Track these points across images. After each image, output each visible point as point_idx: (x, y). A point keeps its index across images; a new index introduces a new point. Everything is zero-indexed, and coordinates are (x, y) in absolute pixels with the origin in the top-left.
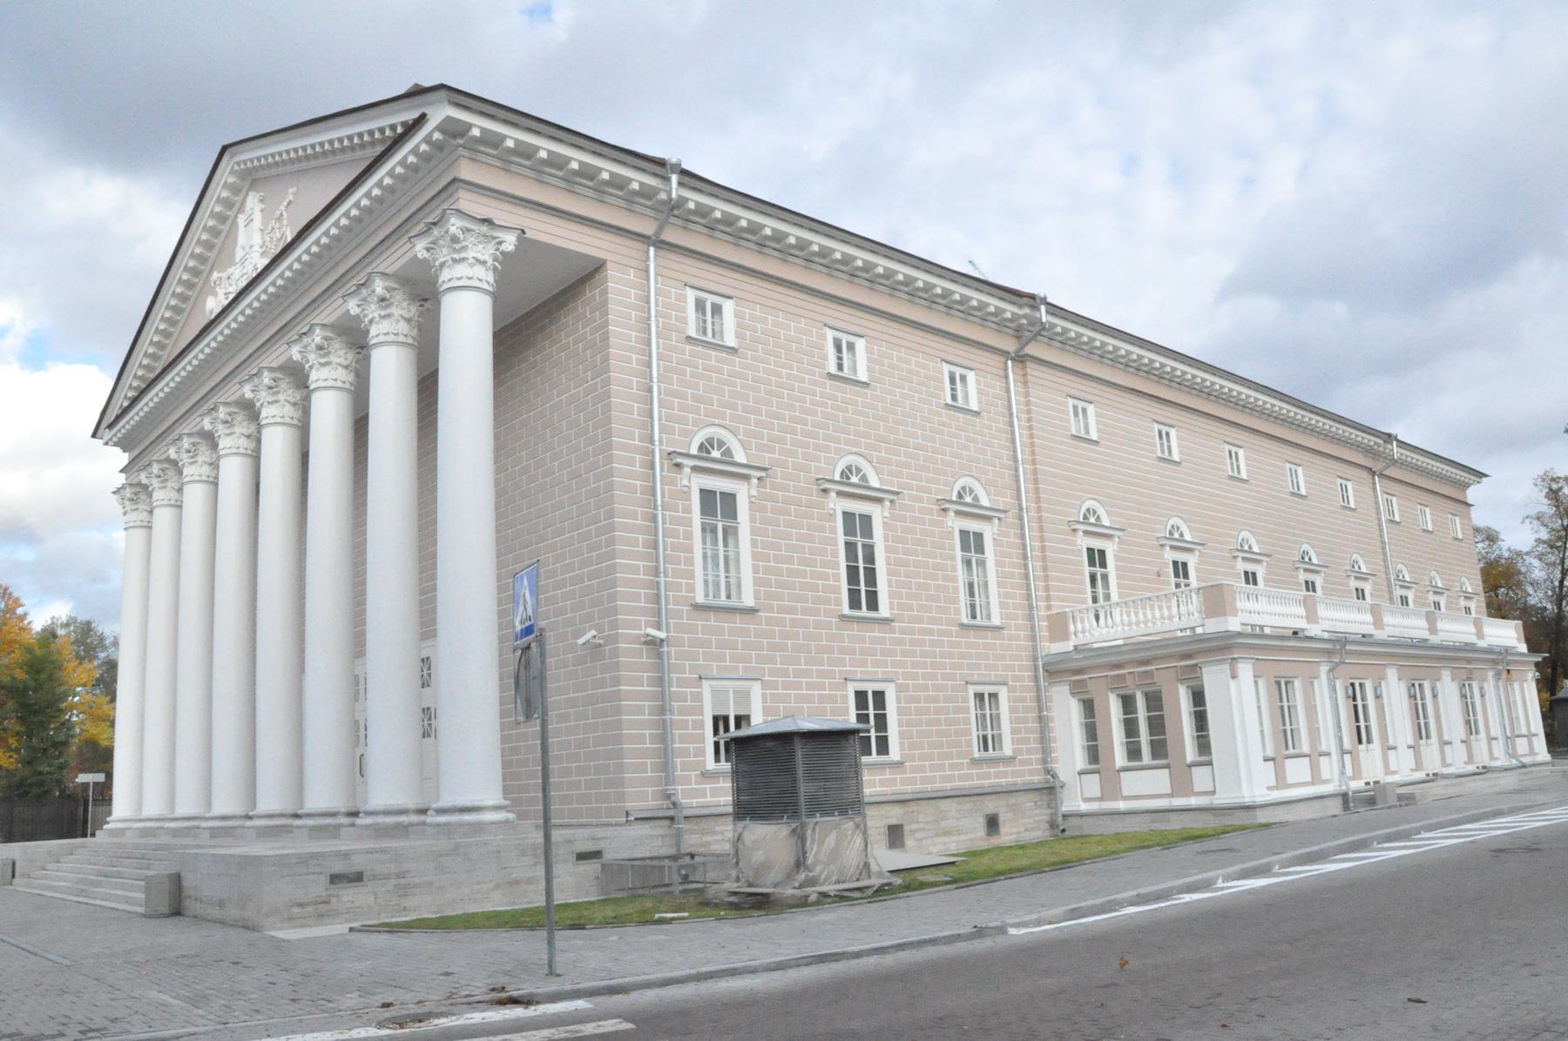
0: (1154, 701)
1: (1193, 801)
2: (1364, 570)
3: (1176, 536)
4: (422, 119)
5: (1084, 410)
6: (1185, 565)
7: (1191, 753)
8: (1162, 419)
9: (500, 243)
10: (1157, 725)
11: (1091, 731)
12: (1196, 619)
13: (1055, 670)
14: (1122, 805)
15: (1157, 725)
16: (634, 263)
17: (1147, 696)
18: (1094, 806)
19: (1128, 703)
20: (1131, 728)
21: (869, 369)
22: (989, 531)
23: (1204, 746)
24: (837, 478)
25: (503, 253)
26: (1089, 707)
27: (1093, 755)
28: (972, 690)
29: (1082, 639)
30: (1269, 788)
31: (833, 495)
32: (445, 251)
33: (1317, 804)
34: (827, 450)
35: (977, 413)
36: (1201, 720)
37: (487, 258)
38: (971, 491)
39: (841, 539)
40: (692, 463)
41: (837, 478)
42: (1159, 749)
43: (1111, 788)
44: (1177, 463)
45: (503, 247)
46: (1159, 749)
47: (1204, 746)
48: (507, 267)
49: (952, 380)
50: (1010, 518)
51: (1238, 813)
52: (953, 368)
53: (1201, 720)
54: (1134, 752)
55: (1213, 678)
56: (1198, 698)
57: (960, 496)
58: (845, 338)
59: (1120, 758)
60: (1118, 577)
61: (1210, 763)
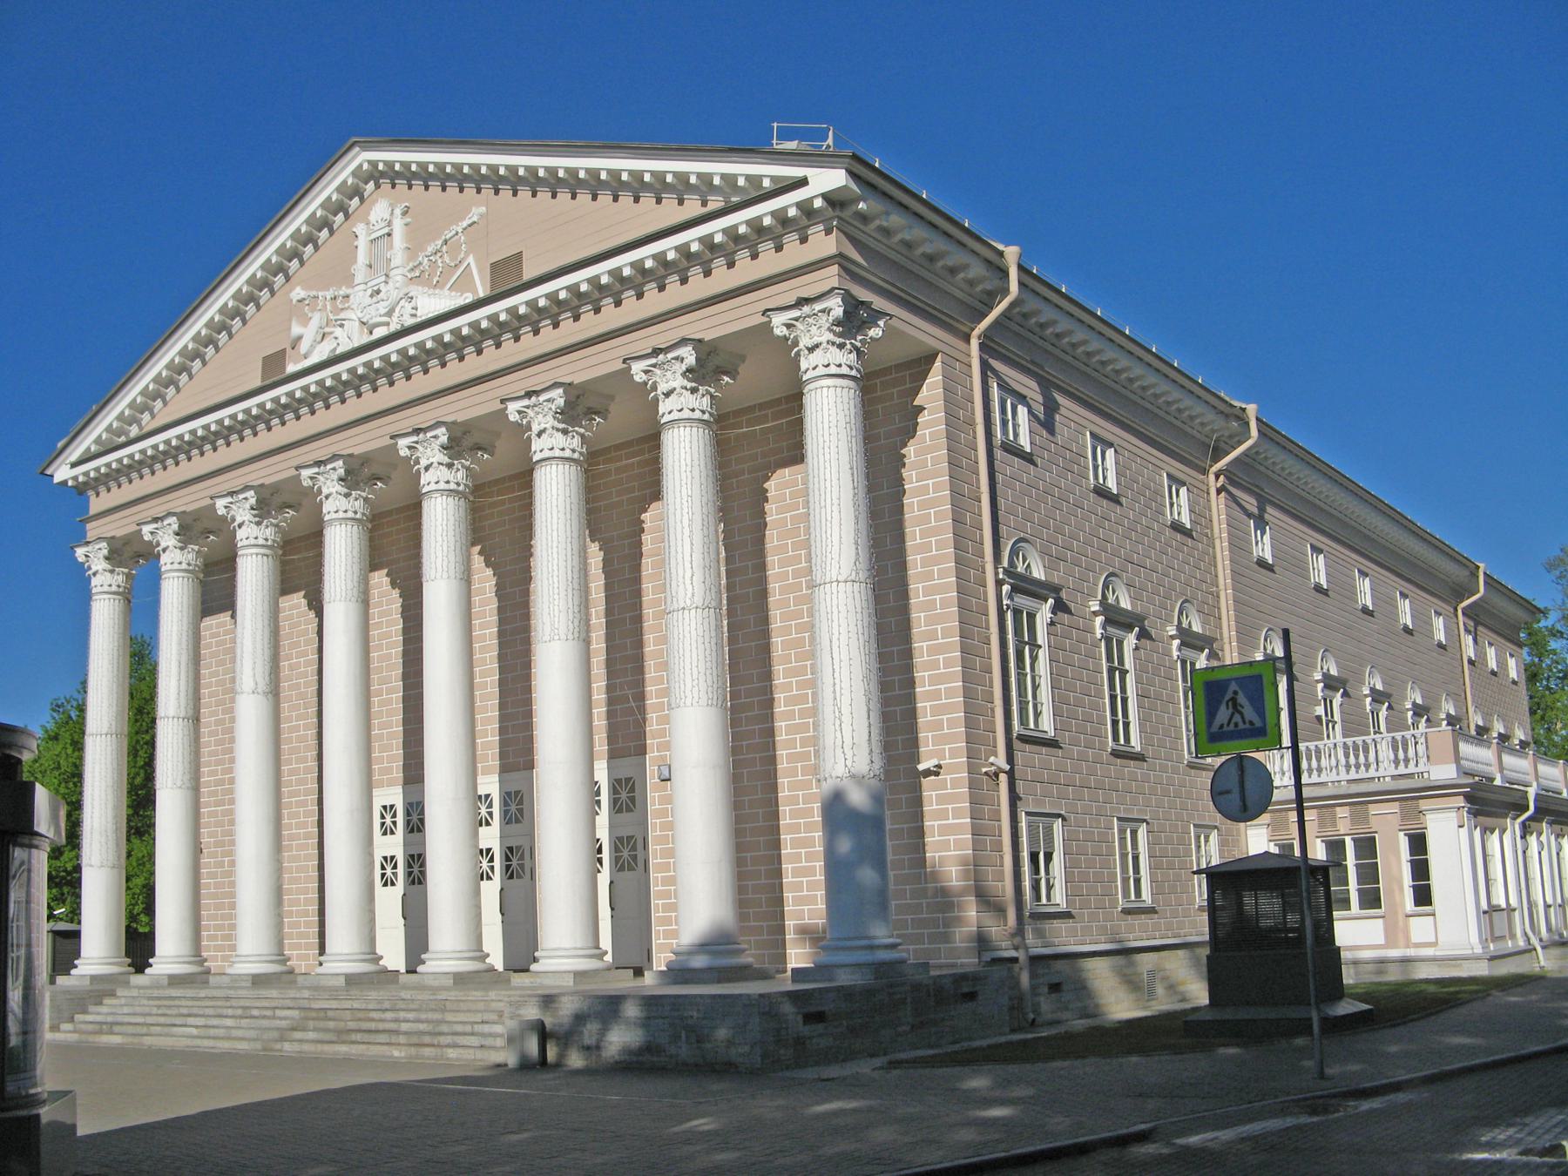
4: (803, 182)
23: (1423, 896)
53: (1421, 870)
56: (1418, 843)
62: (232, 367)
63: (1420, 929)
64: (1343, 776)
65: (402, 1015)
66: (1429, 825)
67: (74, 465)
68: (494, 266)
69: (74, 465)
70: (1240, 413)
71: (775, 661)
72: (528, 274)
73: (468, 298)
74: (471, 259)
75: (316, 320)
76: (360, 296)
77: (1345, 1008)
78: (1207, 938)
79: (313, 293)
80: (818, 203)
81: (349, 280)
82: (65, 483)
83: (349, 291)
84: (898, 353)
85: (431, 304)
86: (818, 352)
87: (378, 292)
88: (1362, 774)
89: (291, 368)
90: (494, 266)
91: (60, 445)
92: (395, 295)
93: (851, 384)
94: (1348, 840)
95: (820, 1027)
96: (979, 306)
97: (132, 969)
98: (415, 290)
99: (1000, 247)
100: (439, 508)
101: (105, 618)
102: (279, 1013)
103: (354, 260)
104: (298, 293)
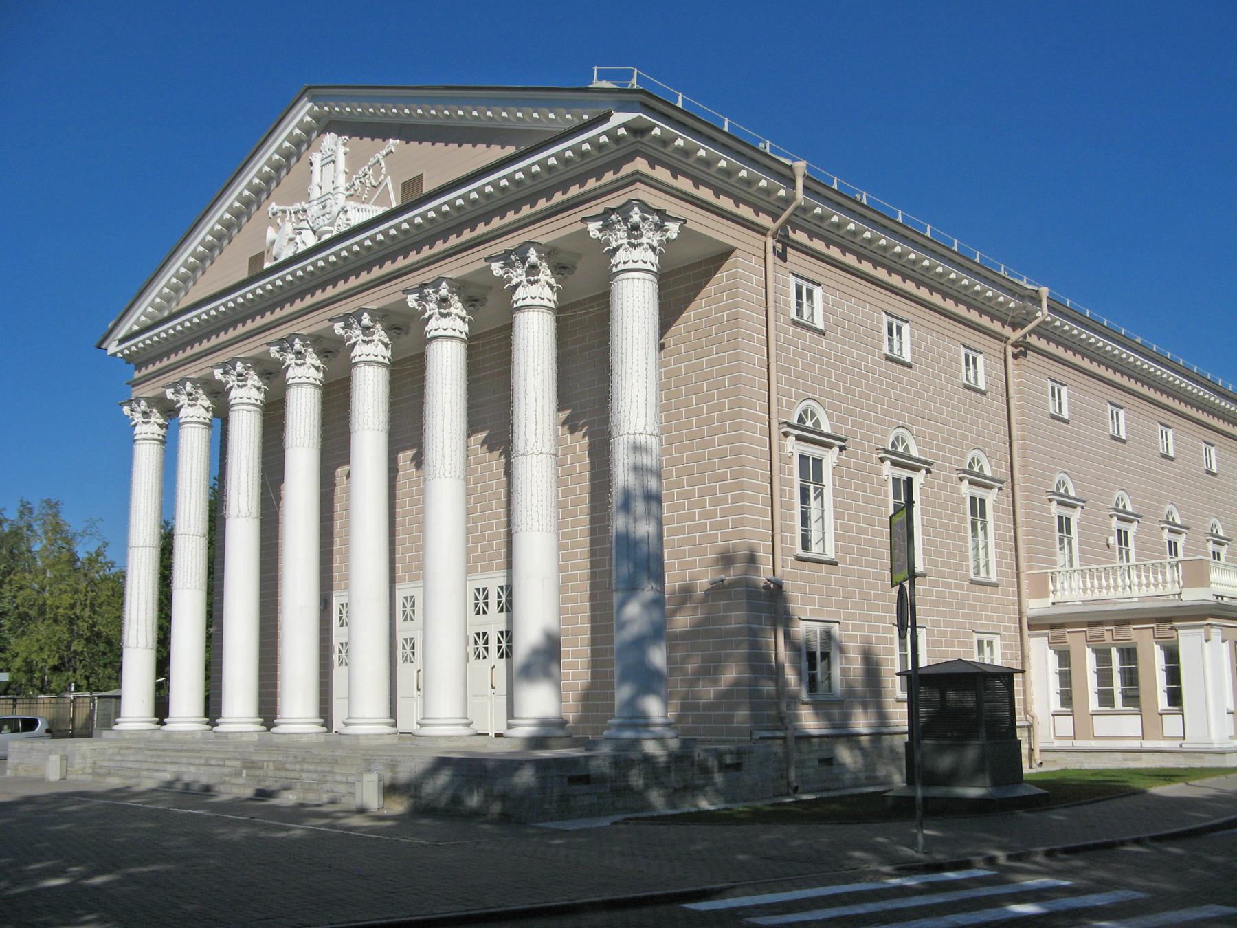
0: (1129, 655)
1: (1163, 745)
2: (1129, 509)
3: (1062, 491)
5: (974, 359)
6: (982, 501)
7: (1162, 702)
8: (968, 342)
9: (667, 231)
10: (1131, 677)
11: (1065, 678)
12: (1171, 589)
13: (1037, 625)
14: (1094, 744)
15: (1131, 677)
16: (998, 354)
17: (1121, 651)
18: (1067, 744)
19: (1103, 657)
20: (1104, 678)
21: (913, 351)
22: (991, 497)
23: (1175, 697)
24: (795, 422)
25: (668, 240)
26: (1064, 657)
27: (1067, 699)
28: (976, 637)
29: (1059, 597)
30: (1231, 737)
31: (888, 463)
32: (620, 234)
33: (1160, 756)
34: (882, 422)
35: (984, 393)
36: (1174, 675)
37: (655, 244)
38: (813, 415)
39: (797, 483)
40: (797, 432)
41: (795, 422)
42: (1132, 698)
43: (1083, 728)
44: (1067, 422)
45: (668, 235)
46: (1132, 698)
47: (1175, 697)
48: (665, 250)
49: (799, 294)
50: (1006, 488)
51: (1207, 756)
52: (801, 282)
53: (1174, 675)
54: (1106, 698)
55: (1188, 640)
56: (1172, 656)
57: (800, 419)
58: (895, 323)
59: (1093, 703)
60: (1080, 543)
61: (1182, 713)
62: (230, 267)
63: (1172, 724)
64: (1081, 596)
65: (306, 767)
66: (1180, 638)
67: (122, 341)
68: (404, 185)
69: (122, 341)
70: (1034, 294)
71: (336, 500)
72: (427, 188)
73: (380, 211)
74: (389, 181)
75: (288, 228)
76: (314, 209)
77: (1022, 791)
78: (906, 728)
79: (283, 207)
80: (622, 131)
81: (307, 197)
82: (114, 355)
83: (306, 206)
84: (692, 253)
85: (358, 217)
86: (639, 250)
87: (324, 207)
88: (1096, 595)
89: (267, 265)
90: (404, 185)
91: (110, 325)
92: (336, 209)
93: (648, 276)
94: (1114, 651)
95: (583, 788)
96: (776, 210)
97: (264, 728)
98: (351, 205)
99: (788, 162)
100: (371, 377)
101: (146, 458)
102: (228, 763)
103: (310, 181)
104: (274, 207)
